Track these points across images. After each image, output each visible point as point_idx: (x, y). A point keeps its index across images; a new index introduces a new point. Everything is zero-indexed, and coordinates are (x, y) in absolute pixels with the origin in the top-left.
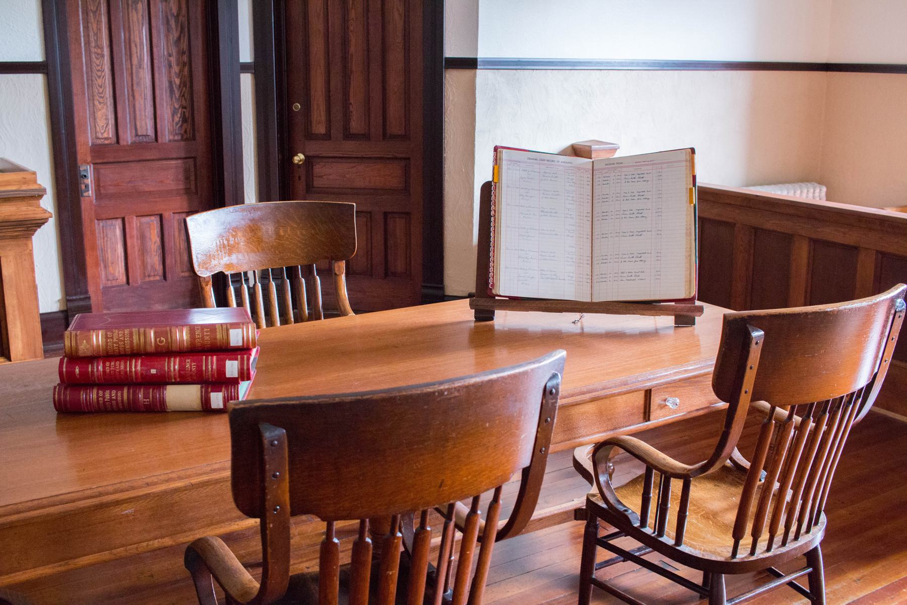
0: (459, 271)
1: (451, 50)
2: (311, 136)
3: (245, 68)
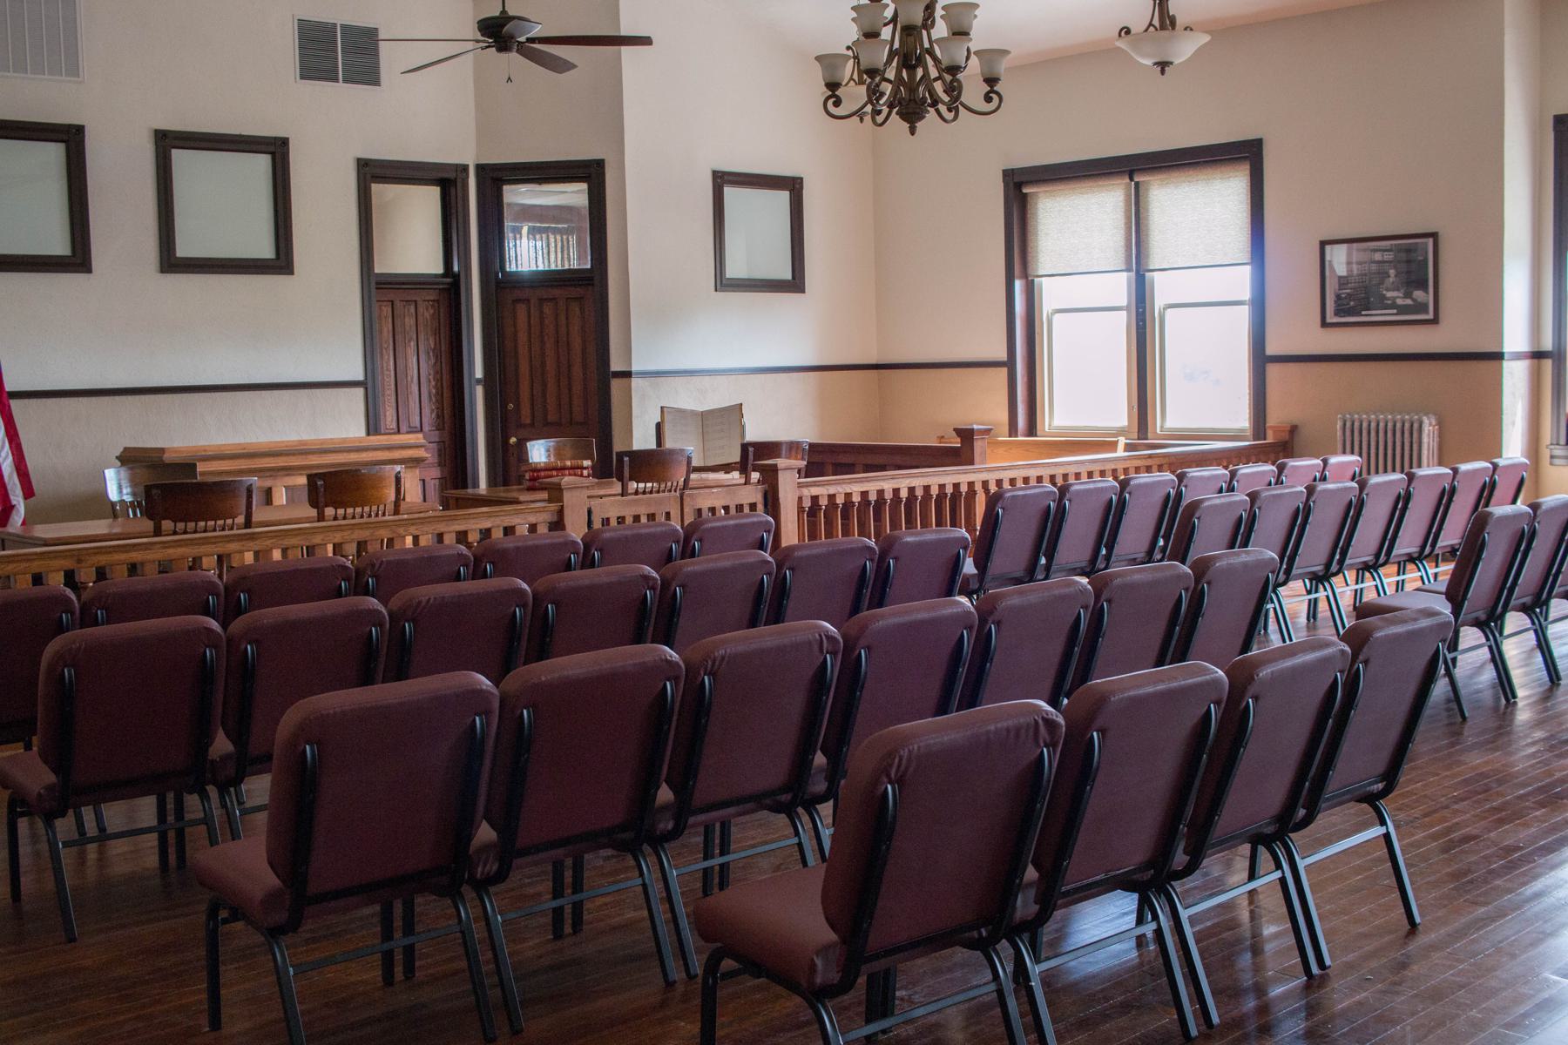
0: (501, 492)
1: (615, 366)
2: (520, 426)
3: (478, 381)
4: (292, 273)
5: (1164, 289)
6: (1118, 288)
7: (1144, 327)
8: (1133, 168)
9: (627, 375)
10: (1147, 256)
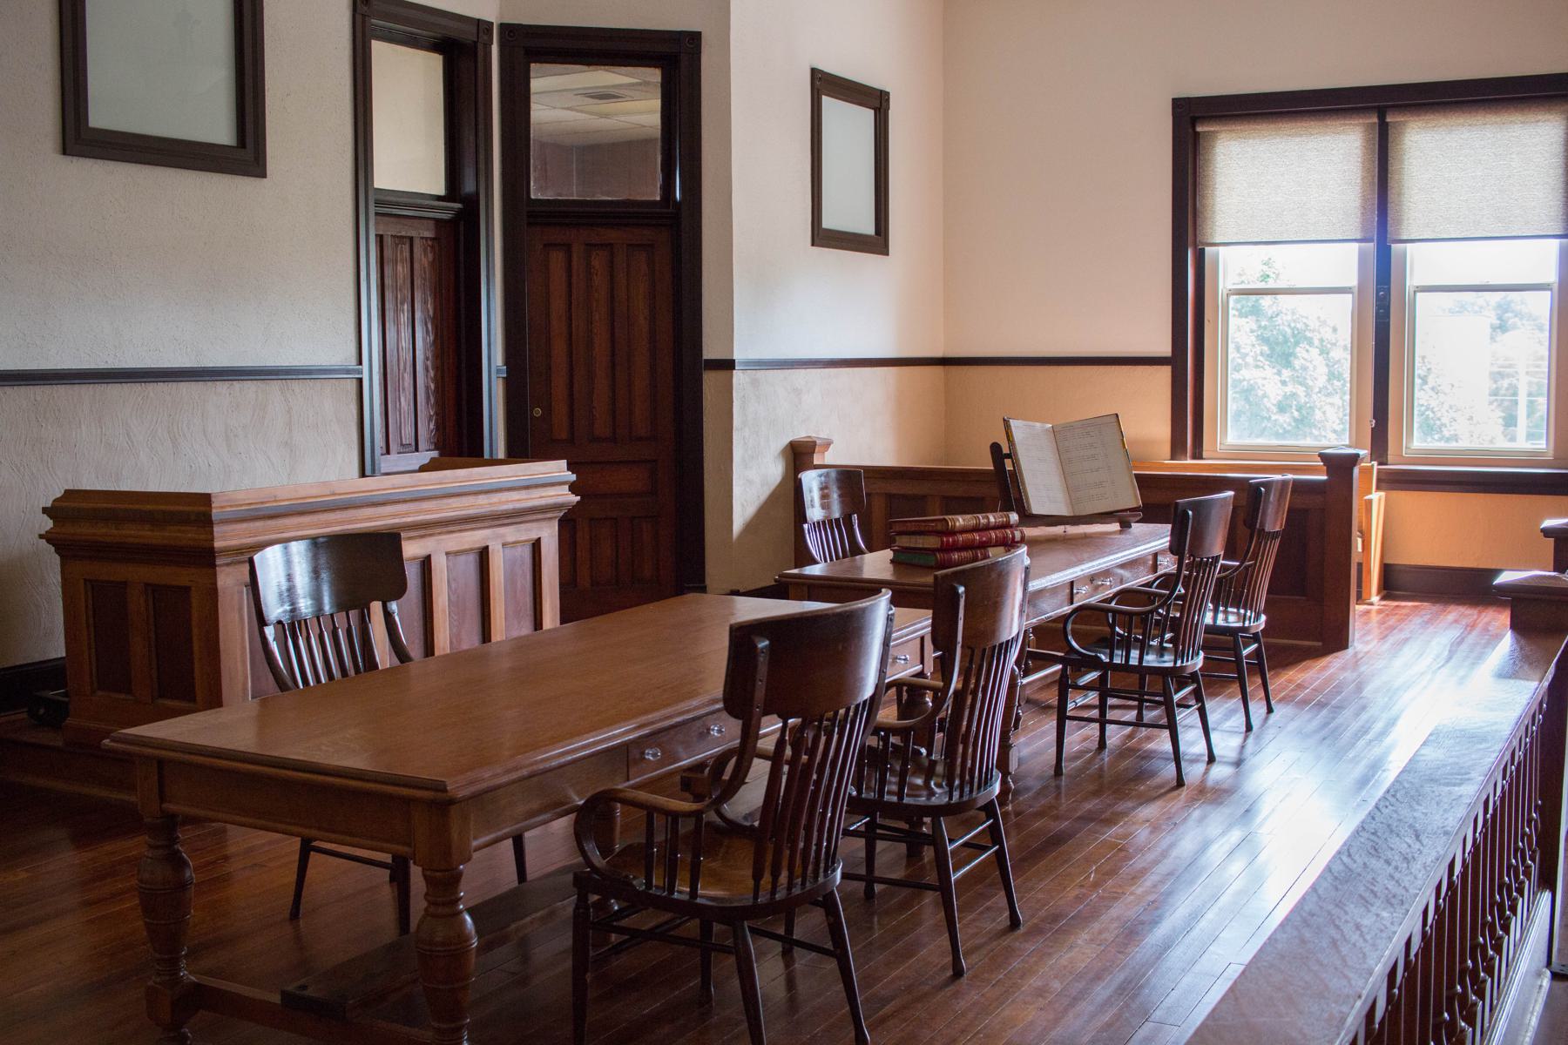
1: (710, 352)
4: (264, 176)
5: (1422, 263)
6: (1344, 263)
7: (1387, 315)
8: (1382, 107)
9: (729, 365)
10: (1399, 222)
